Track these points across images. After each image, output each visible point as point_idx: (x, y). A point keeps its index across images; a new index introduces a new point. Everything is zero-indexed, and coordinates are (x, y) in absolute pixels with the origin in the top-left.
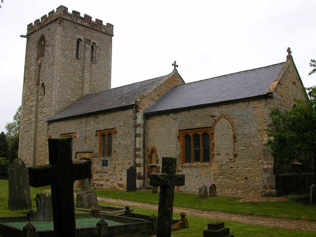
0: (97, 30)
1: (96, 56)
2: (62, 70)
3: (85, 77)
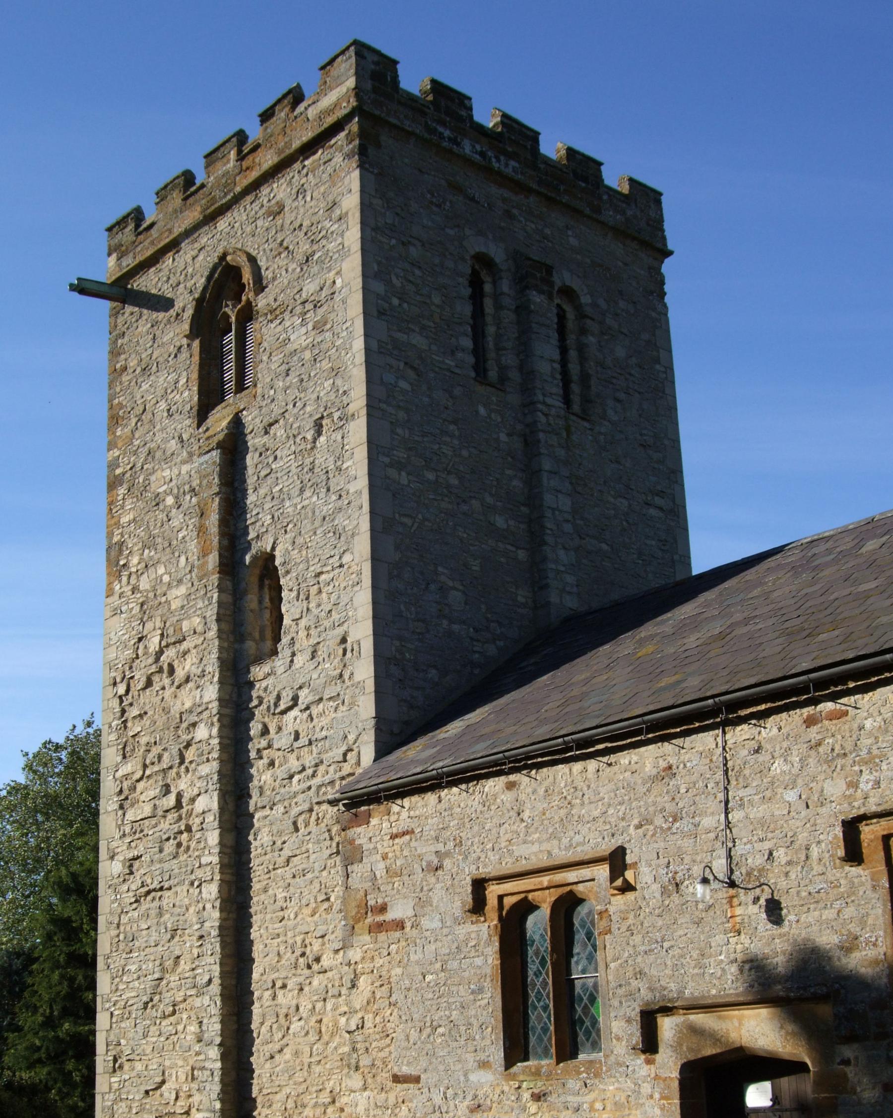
0: (576, 212)
1: (585, 378)
2: (401, 454)
3: (549, 499)
